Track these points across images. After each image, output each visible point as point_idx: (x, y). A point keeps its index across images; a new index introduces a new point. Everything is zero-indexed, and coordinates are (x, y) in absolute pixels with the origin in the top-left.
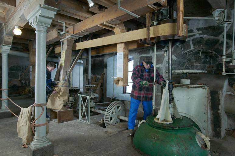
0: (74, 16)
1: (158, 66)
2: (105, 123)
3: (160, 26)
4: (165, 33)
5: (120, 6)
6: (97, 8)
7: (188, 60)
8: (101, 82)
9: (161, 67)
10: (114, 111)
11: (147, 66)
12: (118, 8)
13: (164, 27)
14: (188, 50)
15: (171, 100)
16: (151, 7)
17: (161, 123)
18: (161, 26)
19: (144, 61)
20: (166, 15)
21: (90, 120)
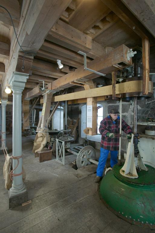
3: (125, 83)
4: (130, 90)
5: (86, 68)
7: (152, 109)
8: (76, 125)
9: (126, 115)
11: (114, 117)
12: (85, 68)
14: (152, 101)
15: (137, 153)
16: (116, 66)
19: (111, 113)
20: (131, 72)
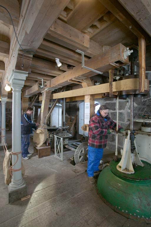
0: (49, 74)
1: (120, 111)
2: (75, 161)
4: (126, 88)
5: (83, 66)
6: (66, 66)
8: (74, 122)
9: (123, 112)
10: (83, 151)
13: (126, 82)
16: (113, 65)
17: (123, 173)
18: (123, 82)
21: (63, 156)
